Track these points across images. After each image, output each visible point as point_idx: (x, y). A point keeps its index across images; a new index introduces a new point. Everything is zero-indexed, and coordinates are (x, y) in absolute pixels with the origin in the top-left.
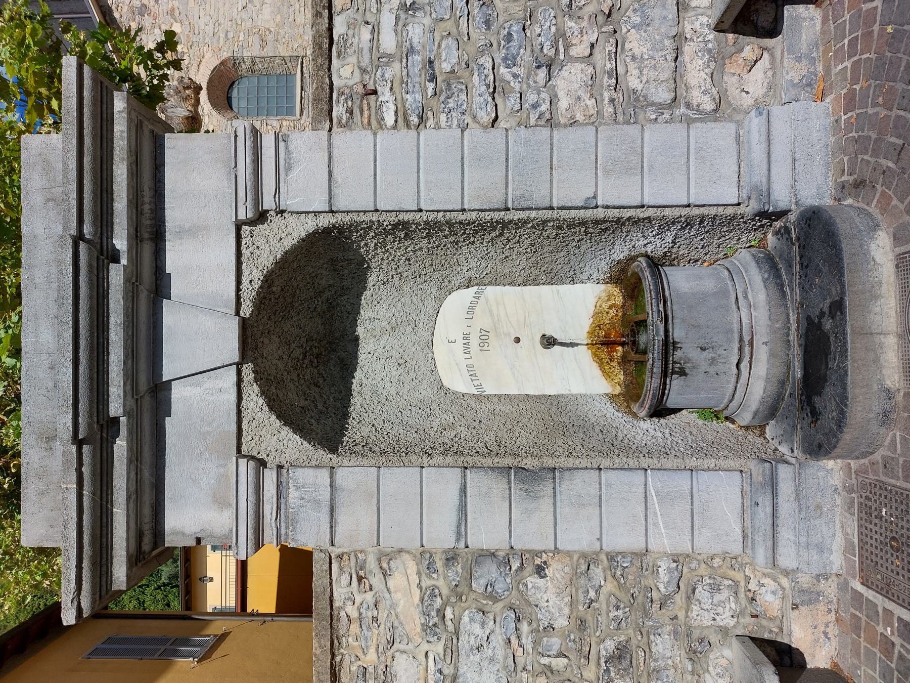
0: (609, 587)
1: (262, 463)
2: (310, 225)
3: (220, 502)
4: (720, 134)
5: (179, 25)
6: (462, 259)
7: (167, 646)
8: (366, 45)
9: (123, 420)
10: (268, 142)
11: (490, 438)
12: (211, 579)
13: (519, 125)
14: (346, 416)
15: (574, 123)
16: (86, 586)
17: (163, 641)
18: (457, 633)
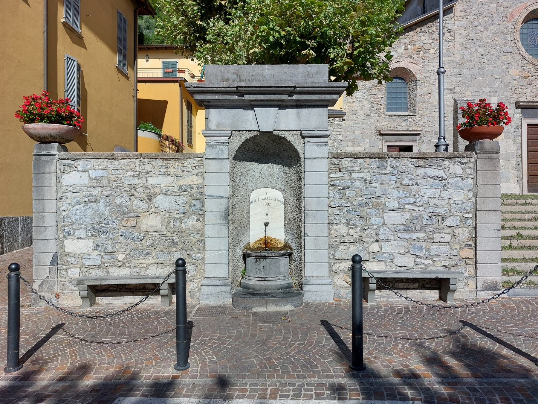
0: (194, 240)
1: (230, 138)
2: (301, 152)
3: (218, 125)
4: (325, 271)
5: (434, 52)
6: (292, 197)
7: (123, 50)
8: (354, 169)
9: (243, 98)
10: (325, 139)
11: (237, 205)
12: (147, 61)
13: (330, 214)
14: (243, 161)
15: (330, 230)
16: (196, 89)
17: (125, 48)
18: (180, 195)
